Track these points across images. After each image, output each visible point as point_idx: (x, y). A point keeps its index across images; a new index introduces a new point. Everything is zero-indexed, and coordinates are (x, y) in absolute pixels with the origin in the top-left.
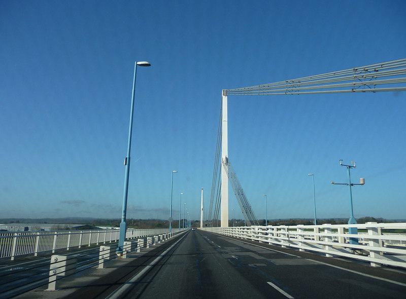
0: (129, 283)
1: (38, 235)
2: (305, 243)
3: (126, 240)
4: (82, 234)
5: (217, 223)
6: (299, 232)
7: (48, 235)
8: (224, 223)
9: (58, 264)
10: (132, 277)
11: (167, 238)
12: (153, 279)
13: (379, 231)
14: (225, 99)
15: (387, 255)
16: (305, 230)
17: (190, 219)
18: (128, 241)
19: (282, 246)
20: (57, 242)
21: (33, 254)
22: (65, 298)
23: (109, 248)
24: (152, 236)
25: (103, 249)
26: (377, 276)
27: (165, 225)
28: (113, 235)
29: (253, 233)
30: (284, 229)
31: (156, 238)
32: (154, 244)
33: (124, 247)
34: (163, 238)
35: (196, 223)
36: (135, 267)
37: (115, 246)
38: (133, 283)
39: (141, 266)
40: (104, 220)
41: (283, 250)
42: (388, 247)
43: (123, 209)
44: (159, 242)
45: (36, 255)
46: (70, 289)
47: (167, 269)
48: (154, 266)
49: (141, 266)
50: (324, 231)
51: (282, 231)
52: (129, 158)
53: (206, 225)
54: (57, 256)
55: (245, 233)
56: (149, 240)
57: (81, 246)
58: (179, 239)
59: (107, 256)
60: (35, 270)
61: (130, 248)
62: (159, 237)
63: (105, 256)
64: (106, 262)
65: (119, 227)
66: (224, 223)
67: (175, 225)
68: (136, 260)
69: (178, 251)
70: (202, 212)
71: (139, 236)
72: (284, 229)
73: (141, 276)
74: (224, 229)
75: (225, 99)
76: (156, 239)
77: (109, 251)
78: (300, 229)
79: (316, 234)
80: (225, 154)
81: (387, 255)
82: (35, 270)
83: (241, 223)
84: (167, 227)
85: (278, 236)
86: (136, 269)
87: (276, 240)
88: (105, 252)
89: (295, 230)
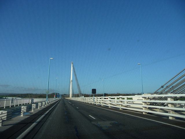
3: (34, 103)
4: (16, 100)
6: (109, 99)
8: (71, 95)
9: (24, 109)
11: (50, 103)
12: (43, 124)
15: (149, 108)
16: (112, 98)
17: (61, 93)
18: (34, 104)
19: (120, 109)
21: (14, 106)
24: (45, 101)
25: (2, 113)
26: (168, 123)
28: (28, 101)
29: (80, 99)
30: (103, 98)
35: (64, 96)
38: (38, 122)
39: (29, 123)
40: (17, 94)
41: (102, 107)
42: (129, 104)
44: (46, 105)
46: (9, 124)
48: (46, 115)
49: (29, 123)
51: (102, 99)
53: (74, 95)
54: (2, 111)
55: (85, 100)
56: (44, 103)
57: (6, 107)
61: (26, 110)
63: (24, 111)
66: (71, 95)
67: (51, 96)
70: (71, 83)
76: (47, 103)
77: (6, 114)
78: (109, 98)
79: (116, 100)
80: (71, 79)
81: (149, 108)
83: (78, 96)
84: (45, 97)
85: (108, 102)
86: (26, 125)
87: (100, 103)
88: (24, 109)
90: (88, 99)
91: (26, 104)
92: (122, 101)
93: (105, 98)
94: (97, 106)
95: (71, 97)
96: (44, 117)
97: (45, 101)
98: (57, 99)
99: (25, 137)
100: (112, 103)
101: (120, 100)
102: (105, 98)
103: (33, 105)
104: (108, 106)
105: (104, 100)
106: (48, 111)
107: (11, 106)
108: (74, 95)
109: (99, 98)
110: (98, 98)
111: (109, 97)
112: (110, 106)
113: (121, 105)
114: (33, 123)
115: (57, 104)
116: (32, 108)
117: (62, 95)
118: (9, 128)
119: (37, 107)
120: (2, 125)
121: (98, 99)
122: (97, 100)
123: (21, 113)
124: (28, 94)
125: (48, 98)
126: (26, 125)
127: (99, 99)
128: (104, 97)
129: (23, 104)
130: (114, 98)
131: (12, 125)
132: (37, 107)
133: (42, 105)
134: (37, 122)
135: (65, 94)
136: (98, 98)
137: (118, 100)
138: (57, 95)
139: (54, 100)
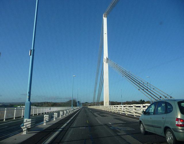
0: (61, 128)
1: (6, 110)
2: (136, 112)
5: (102, 104)
7: (9, 110)
9: (27, 122)
10: (67, 121)
11: (71, 111)
13: (128, 106)
14: (105, 20)
16: (137, 107)
17: (82, 102)
19: (134, 116)
20: (6, 114)
21: (13, 118)
22: (22, 143)
23: (48, 115)
24: (66, 110)
27: (146, 112)
29: (120, 109)
30: (127, 106)
31: (68, 111)
32: (64, 115)
33: (54, 115)
34: (69, 112)
35: (85, 104)
36: (59, 124)
37: (58, 112)
38: (62, 128)
43: (28, 91)
44: (67, 114)
45: (14, 118)
47: (71, 132)
50: (145, 107)
52: (34, 50)
58: (71, 117)
59: (29, 126)
60: (15, 126)
61: (48, 119)
62: (67, 112)
63: (46, 119)
64: (28, 130)
65: (24, 105)
68: (36, 134)
69: (68, 137)
71: (55, 111)
72: (127, 106)
73: (53, 139)
74: (106, 107)
75: (105, 20)
76: (68, 111)
77: (30, 122)
82: (15, 126)
87: (124, 111)
88: (46, 117)
89: (132, 107)
90: (111, 107)
91: (55, 111)
92: (116, 108)
93: (129, 107)
94: (126, 116)
95: (108, 103)
96: (73, 118)
97: (66, 110)
98: (75, 108)
99: (52, 142)
100: (136, 111)
101: (116, 107)
102: (129, 107)
103: (60, 112)
104: (133, 115)
105: (128, 108)
106: (57, 133)
107: (38, 114)
108: (112, 103)
109: (114, 107)
110: (122, 107)
111: (134, 105)
112: (135, 114)
113: (135, 112)
114: (56, 131)
115: (78, 113)
116: (44, 120)
117: (83, 104)
118: (27, 139)
119: (59, 116)
120: (26, 134)
121: (121, 108)
122: (121, 108)
123: (44, 122)
124: (45, 103)
125: (73, 106)
126: (49, 133)
127: (113, 107)
128: (116, 105)
129: (45, 113)
130: (140, 107)
131: (35, 133)
132: (59, 116)
133: (63, 114)
134: (61, 128)
135: (86, 103)
136: (122, 107)
137: (125, 108)
138: (75, 103)
139: (70, 110)
